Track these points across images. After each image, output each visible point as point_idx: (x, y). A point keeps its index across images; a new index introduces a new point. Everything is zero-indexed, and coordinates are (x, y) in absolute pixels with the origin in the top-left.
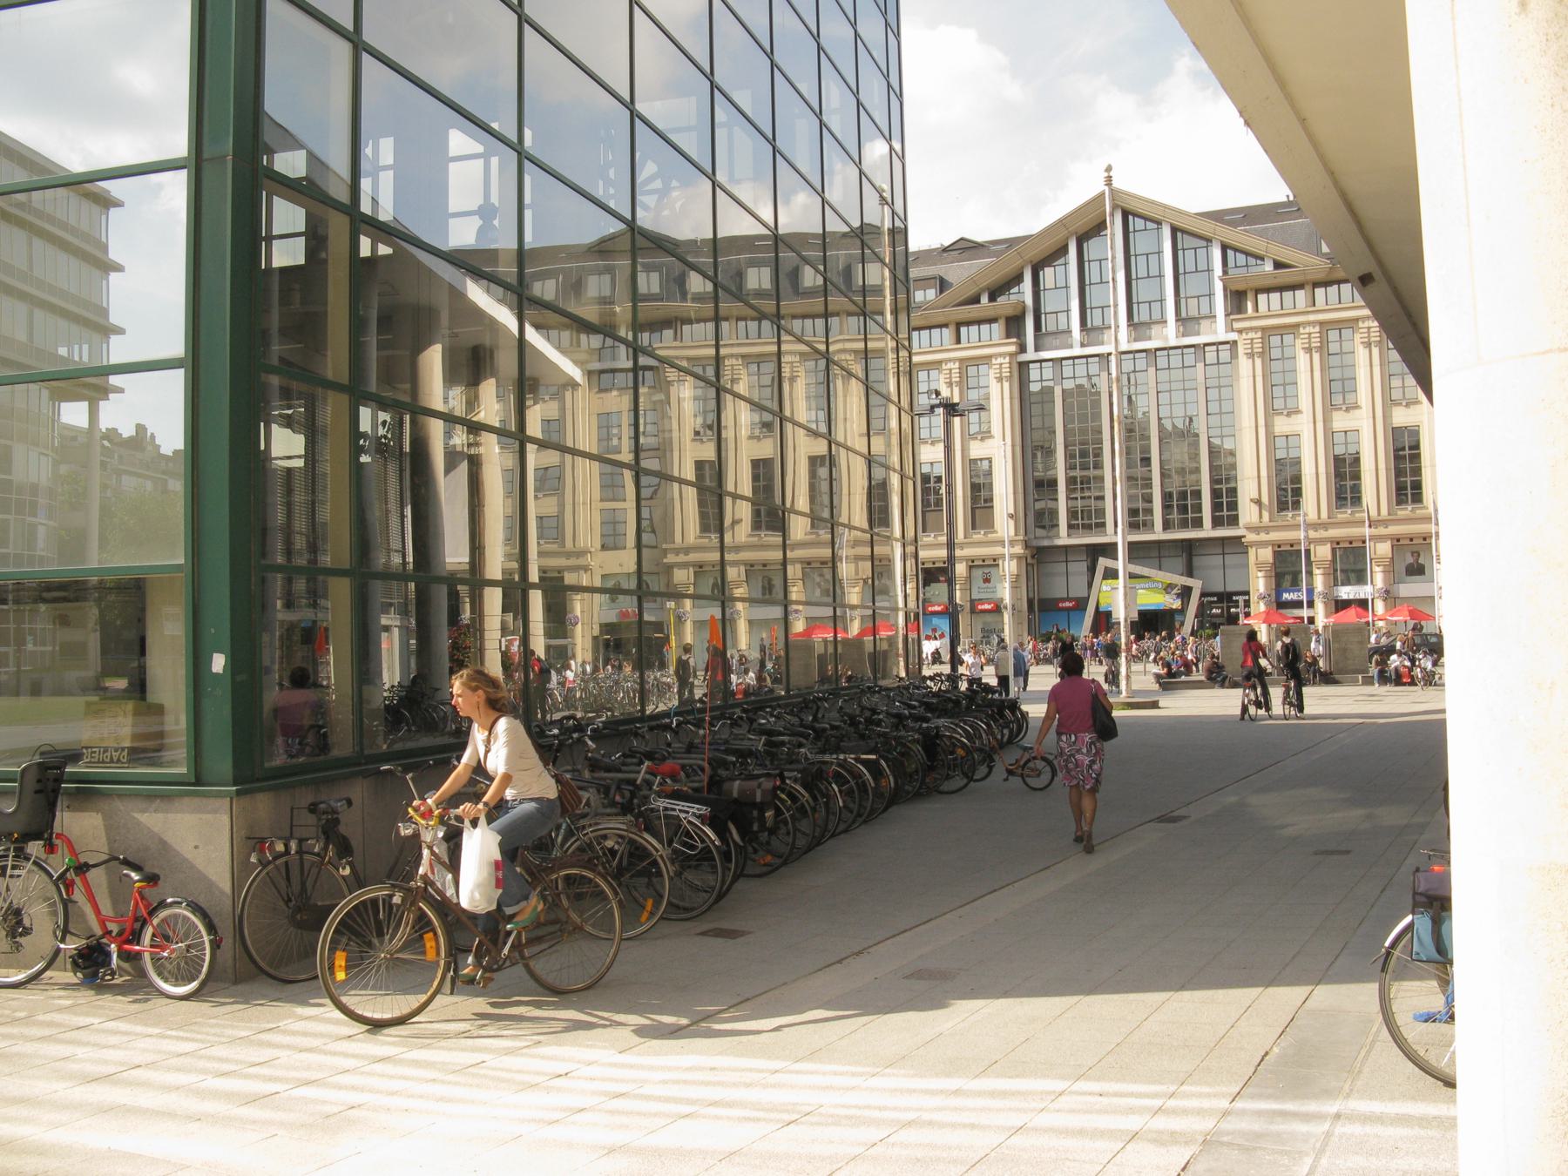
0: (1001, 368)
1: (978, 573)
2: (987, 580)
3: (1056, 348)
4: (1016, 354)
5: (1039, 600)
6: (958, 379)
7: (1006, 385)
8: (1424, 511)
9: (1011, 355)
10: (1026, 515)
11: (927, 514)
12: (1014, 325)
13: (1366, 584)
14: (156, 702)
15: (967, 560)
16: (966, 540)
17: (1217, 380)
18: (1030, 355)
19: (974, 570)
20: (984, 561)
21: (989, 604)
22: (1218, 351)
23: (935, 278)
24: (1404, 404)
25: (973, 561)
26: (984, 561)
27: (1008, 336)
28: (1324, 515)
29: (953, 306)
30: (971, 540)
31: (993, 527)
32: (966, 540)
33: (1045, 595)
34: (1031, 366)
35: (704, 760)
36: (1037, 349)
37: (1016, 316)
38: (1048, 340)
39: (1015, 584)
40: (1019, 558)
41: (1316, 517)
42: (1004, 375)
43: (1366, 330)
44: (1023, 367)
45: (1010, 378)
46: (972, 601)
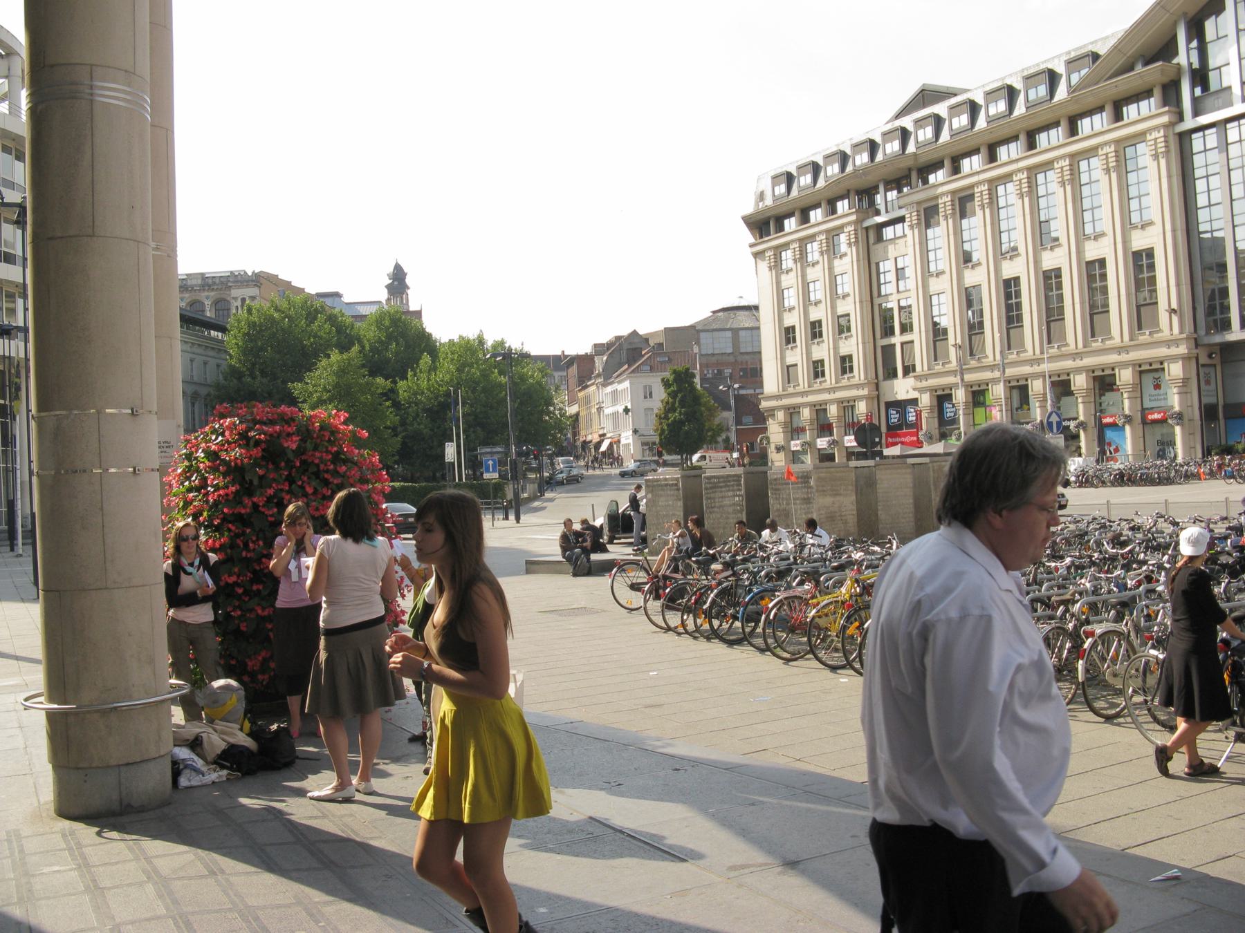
0: (1156, 144)
1: (1148, 380)
2: (1157, 387)
3: (1219, 109)
4: (1171, 125)
5: (1225, 406)
6: (1114, 164)
7: (1163, 162)
8: (1160, 335)
9: (1166, 127)
10: (1194, 309)
11: (1095, 316)
12: (1170, 93)
13: (1205, 406)
14: (912, 524)
15: (1087, 371)
16: (1132, 343)
17: (1006, 217)
18: (1189, 123)
19: (1144, 376)
20: (1151, 365)
21: (1159, 413)
22: (1239, 126)
23: (1088, 55)
24: (1140, 227)
25: (1140, 366)
26: (1151, 365)
27: (1165, 105)
28: (1080, 345)
29: (1110, 78)
30: (841, 385)
31: (1158, 325)
32: (1132, 343)
33: (1232, 400)
34: (1194, 136)
35: (1232, 611)
36: (1196, 113)
37: (1172, 81)
38: (1209, 102)
39: (1185, 389)
40: (1185, 359)
41: (1120, 341)
42: (1159, 151)
43: (1059, 170)
44: (1184, 139)
45: (1167, 153)
46: (1143, 410)
